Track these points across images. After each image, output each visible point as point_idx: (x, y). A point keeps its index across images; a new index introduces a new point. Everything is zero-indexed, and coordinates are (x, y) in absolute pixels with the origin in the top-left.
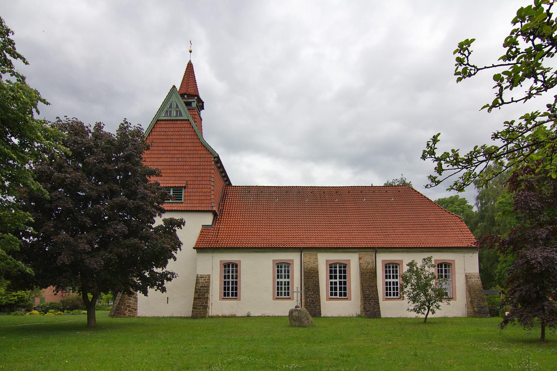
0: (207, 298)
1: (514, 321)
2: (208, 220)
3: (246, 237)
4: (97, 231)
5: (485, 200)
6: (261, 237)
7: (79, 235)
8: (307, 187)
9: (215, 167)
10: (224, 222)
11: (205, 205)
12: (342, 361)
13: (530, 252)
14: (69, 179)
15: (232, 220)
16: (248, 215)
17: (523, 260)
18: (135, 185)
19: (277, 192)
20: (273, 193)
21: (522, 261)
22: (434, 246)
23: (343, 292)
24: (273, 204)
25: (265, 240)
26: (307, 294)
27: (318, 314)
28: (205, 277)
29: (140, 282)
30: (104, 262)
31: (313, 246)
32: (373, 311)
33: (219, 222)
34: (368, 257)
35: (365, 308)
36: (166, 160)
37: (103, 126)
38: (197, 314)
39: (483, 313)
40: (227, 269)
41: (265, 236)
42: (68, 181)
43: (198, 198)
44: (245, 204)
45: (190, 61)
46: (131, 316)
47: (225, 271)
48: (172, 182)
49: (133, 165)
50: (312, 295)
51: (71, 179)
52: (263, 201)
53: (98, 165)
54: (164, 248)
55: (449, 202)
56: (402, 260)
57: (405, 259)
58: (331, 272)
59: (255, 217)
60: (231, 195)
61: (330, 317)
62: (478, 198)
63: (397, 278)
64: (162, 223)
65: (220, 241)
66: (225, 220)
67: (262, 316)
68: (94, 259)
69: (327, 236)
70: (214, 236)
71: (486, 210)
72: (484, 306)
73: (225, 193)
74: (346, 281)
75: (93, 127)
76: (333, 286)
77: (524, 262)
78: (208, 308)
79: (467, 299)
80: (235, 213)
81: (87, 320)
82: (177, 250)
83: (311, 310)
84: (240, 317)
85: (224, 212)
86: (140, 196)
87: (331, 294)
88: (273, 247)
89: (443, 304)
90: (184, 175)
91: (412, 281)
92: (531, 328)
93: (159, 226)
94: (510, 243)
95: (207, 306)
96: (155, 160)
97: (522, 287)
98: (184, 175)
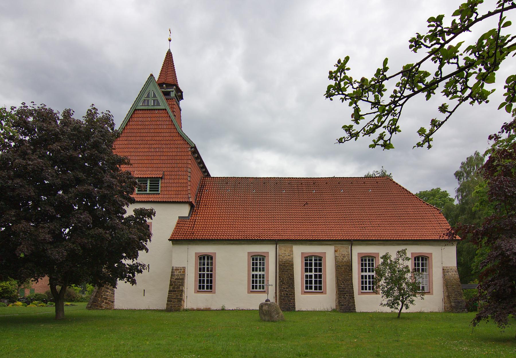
0: (182, 291)
1: (487, 318)
2: (184, 211)
5: (466, 192)
6: (236, 228)
7: (41, 225)
8: (284, 178)
9: (192, 157)
10: (201, 213)
13: (506, 242)
14: (30, 166)
16: (225, 206)
17: (498, 252)
18: (102, 173)
19: (255, 183)
21: (497, 253)
22: (410, 239)
23: (318, 285)
24: (250, 195)
25: (240, 232)
27: (292, 308)
28: (180, 270)
32: (348, 305)
33: (196, 213)
34: (344, 250)
35: (339, 302)
37: (72, 112)
38: (171, 307)
39: (460, 308)
40: (202, 261)
41: (241, 228)
42: (30, 168)
45: (169, 50)
46: (108, 308)
47: (200, 263)
48: (149, 172)
49: (99, 152)
50: (287, 288)
54: (130, 238)
55: (430, 194)
56: (379, 253)
57: (380, 251)
58: (306, 264)
59: (232, 209)
60: (209, 187)
61: (305, 311)
62: (458, 190)
63: (373, 271)
64: (133, 214)
65: (195, 233)
66: (201, 211)
69: (303, 228)
71: (467, 203)
72: (461, 301)
73: (203, 184)
74: (321, 275)
76: (309, 279)
77: (498, 254)
78: (182, 302)
79: (444, 294)
81: (55, 313)
83: (286, 303)
85: (201, 204)
86: (106, 184)
87: (307, 288)
88: (248, 239)
89: (417, 299)
91: (386, 274)
92: (505, 325)
93: (129, 216)
94: (484, 234)
95: (181, 299)
96: (132, 150)
97: (496, 281)
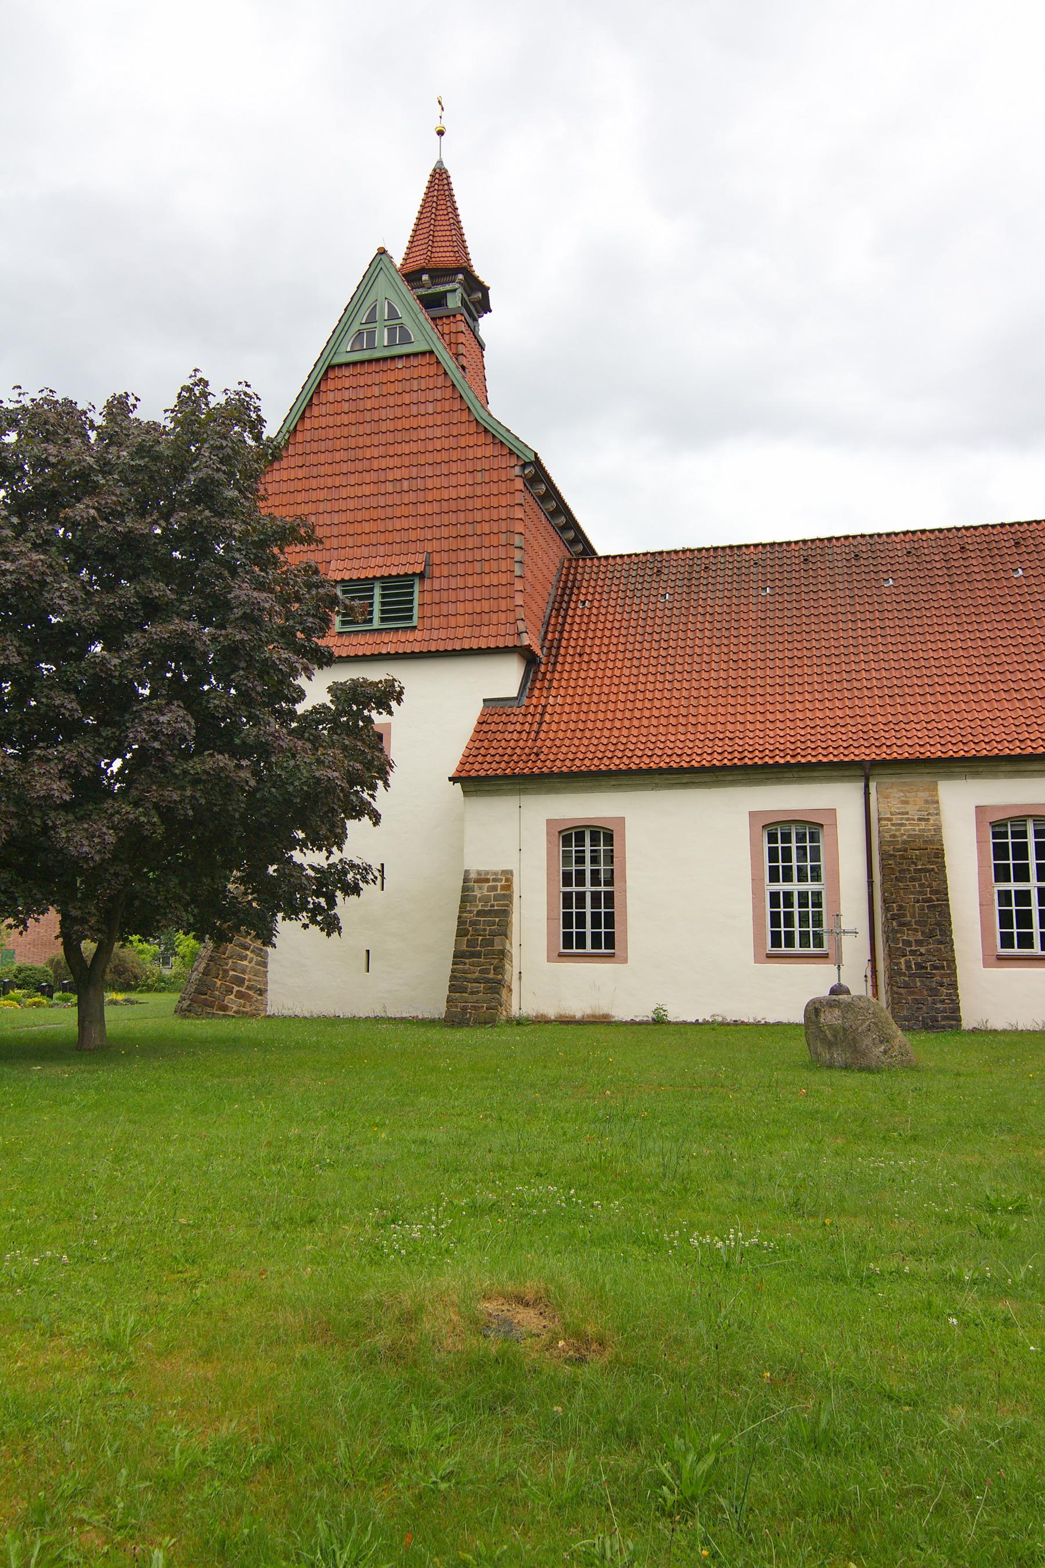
3: (644, 731)
4: (100, 736)
6: (700, 728)
7: (38, 752)
9: (528, 496)
11: (493, 630)
12: (982, 1232)
14: (9, 578)
15: (591, 674)
18: (224, 579)
20: (752, 570)
24: (752, 607)
26: (896, 940)
27: (945, 1018)
28: (494, 880)
29: (254, 899)
30: (117, 834)
31: (916, 752)
33: (546, 684)
36: (358, 491)
37: (134, 402)
38: (464, 1009)
41: (719, 727)
42: (6, 581)
43: (469, 607)
44: (642, 615)
45: (440, 162)
47: (566, 856)
48: (379, 561)
50: (919, 943)
51: (14, 576)
52: (709, 602)
53: (105, 523)
54: (318, 781)
58: (1000, 851)
64: (326, 699)
65: (545, 750)
66: (565, 675)
67: (713, 1022)
68: (86, 826)
70: (524, 736)
75: (100, 408)
78: (504, 992)
80: (604, 649)
81: (77, 1029)
82: (374, 787)
83: (916, 1001)
84: (626, 1023)
86: (238, 612)
88: (750, 763)
90: (420, 534)
96: (321, 495)
98: (420, 534)
